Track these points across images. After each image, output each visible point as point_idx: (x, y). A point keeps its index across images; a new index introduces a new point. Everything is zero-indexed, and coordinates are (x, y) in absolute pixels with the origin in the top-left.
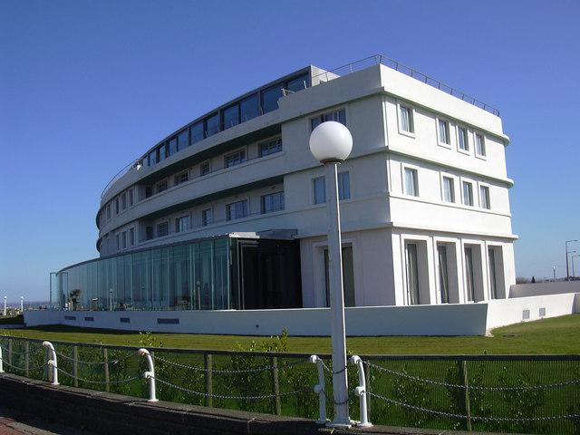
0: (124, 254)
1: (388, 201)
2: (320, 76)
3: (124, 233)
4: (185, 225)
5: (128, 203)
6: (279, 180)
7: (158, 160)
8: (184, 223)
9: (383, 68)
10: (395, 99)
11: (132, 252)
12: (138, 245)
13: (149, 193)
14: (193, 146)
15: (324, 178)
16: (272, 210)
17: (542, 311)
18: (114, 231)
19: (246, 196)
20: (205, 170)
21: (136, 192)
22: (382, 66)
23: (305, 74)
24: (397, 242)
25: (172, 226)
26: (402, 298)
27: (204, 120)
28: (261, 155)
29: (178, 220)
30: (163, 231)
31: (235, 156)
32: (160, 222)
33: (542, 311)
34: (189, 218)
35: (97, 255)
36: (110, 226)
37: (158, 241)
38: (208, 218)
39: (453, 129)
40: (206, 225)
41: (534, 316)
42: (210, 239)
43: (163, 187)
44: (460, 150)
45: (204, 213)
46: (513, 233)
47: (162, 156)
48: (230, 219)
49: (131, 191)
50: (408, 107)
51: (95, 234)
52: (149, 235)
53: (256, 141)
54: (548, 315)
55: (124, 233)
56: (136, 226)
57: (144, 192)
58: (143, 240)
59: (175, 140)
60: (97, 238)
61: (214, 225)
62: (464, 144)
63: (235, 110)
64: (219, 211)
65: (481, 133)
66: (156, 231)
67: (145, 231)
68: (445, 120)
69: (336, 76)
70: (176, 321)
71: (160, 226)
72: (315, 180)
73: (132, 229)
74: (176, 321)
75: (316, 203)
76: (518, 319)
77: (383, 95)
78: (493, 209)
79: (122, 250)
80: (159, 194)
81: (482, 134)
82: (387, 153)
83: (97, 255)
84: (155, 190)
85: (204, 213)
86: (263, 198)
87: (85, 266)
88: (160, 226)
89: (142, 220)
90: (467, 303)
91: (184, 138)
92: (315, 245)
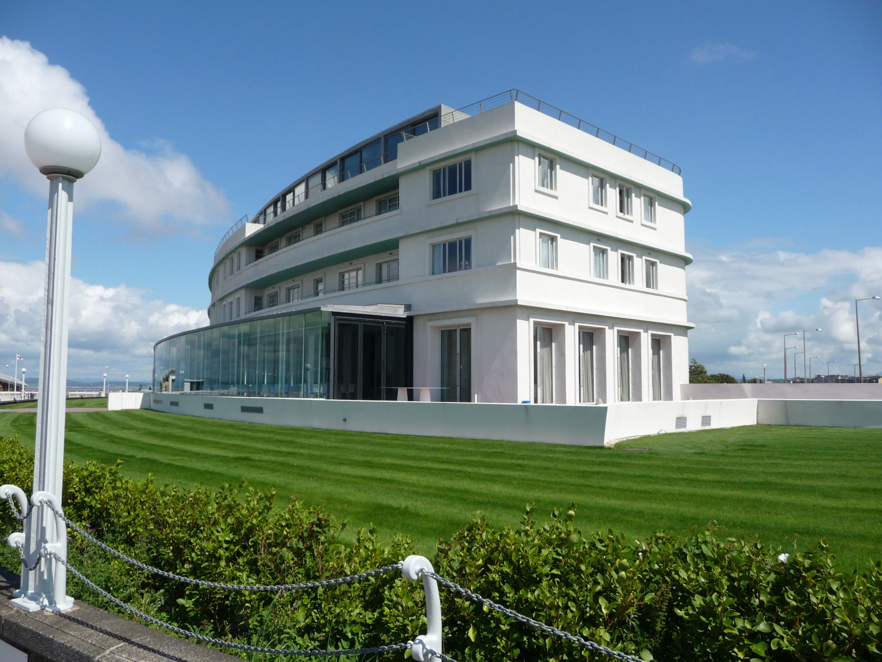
2: (450, 116)
3: (231, 303)
4: (296, 295)
5: (235, 267)
6: (391, 246)
8: (295, 293)
9: (518, 106)
13: (259, 255)
15: (468, 242)
16: (389, 280)
17: (706, 420)
20: (319, 230)
23: (433, 118)
25: (282, 295)
26: (525, 393)
29: (289, 290)
30: (273, 301)
31: (351, 214)
32: (270, 291)
33: (706, 420)
34: (360, 272)
40: (343, 290)
41: (694, 425)
46: (689, 320)
47: (279, 210)
48: (317, 294)
51: (207, 298)
52: (258, 304)
54: (715, 425)
56: (242, 295)
57: (254, 254)
58: (250, 312)
59: (358, 154)
63: (356, 159)
65: (651, 195)
66: (265, 301)
69: (469, 116)
72: (434, 246)
73: (238, 299)
75: (433, 274)
76: (670, 428)
78: (662, 288)
79: (235, 319)
81: (653, 197)
84: (266, 251)
90: (578, 404)
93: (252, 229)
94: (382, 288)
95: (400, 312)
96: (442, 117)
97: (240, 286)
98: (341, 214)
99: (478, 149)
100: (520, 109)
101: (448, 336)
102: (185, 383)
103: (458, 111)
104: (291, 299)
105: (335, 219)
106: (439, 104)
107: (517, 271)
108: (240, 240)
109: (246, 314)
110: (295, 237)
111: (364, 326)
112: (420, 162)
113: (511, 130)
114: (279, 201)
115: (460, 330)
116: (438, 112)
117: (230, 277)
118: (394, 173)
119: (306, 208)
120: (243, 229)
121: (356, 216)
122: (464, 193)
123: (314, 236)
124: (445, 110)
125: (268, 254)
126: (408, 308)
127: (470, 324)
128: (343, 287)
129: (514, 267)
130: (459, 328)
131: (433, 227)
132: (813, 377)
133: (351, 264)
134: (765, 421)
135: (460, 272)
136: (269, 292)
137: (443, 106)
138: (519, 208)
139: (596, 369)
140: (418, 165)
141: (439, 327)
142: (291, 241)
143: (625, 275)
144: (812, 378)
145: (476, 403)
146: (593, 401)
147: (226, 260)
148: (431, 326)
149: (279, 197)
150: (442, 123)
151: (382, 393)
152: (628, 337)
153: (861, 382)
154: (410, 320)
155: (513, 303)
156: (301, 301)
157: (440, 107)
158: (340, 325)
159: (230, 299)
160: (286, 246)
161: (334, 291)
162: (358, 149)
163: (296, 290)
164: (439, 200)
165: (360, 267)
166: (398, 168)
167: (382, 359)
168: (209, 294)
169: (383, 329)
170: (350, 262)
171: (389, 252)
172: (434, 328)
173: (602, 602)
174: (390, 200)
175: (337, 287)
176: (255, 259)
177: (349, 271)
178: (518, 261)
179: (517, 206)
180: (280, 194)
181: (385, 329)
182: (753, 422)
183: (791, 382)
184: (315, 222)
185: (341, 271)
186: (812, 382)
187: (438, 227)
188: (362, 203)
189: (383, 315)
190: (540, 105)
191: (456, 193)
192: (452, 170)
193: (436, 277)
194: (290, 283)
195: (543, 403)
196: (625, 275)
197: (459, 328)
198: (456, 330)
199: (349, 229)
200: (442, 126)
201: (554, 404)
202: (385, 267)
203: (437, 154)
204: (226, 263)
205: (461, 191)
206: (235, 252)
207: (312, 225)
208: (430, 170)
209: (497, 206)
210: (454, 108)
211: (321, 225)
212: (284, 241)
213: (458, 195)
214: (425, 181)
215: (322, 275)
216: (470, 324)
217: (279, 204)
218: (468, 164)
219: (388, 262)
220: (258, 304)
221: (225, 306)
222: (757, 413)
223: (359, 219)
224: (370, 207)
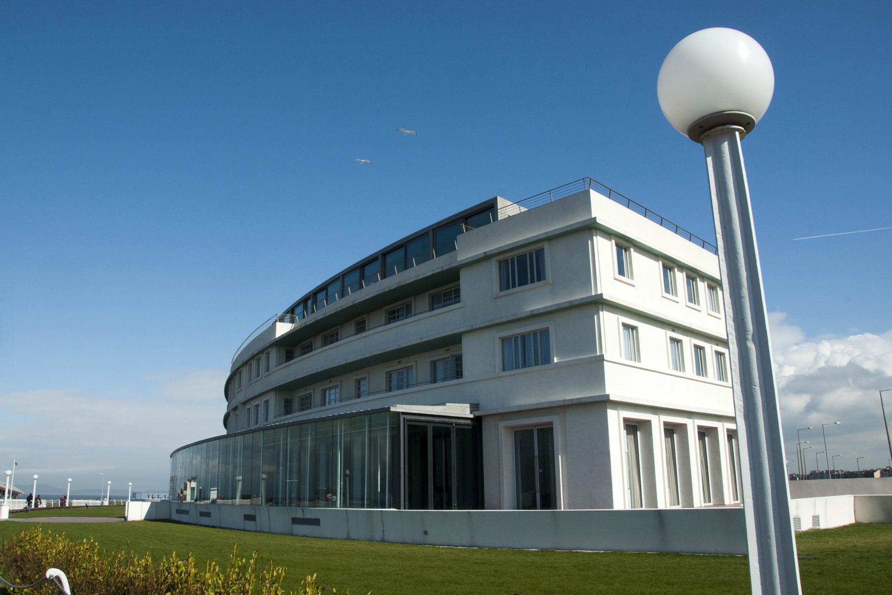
0: (253, 431)
1: (603, 363)
2: (507, 209)
3: (257, 406)
4: (333, 397)
6: (455, 340)
7: (343, 294)
8: (333, 394)
10: (609, 234)
11: (264, 429)
12: (273, 420)
13: (289, 356)
14: (345, 298)
18: (245, 403)
19: (406, 363)
20: (361, 328)
21: (274, 355)
22: (591, 190)
23: (490, 207)
24: (615, 419)
25: (317, 398)
26: (621, 500)
27: (385, 254)
28: (432, 309)
29: (324, 391)
30: (306, 404)
32: (302, 393)
33: (816, 519)
34: (338, 390)
35: (224, 432)
36: (241, 397)
37: (298, 416)
38: (362, 389)
39: (680, 277)
42: (366, 413)
43: (308, 349)
44: (690, 304)
45: (358, 382)
48: (324, 405)
49: (268, 354)
50: (624, 244)
51: (222, 407)
52: (288, 408)
53: (381, 308)
54: (823, 526)
55: (257, 406)
56: (272, 398)
57: (284, 353)
58: (280, 416)
59: (324, 292)
60: (224, 410)
61: (371, 397)
62: (693, 297)
64: (378, 377)
66: (296, 404)
67: (283, 404)
68: (669, 264)
70: (316, 522)
71: (302, 399)
72: (503, 340)
73: (267, 402)
74: (316, 522)
75: (504, 370)
77: (592, 228)
80: (324, 348)
82: (599, 303)
83: (224, 432)
85: (358, 382)
86: (434, 364)
87: (205, 444)
88: (302, 399)
89: (279, 389)
91: (335, 289)
92: (502, 424)
93: (283, 329)
94: (418, 391)
95: (461, 410)
96: (499, 211)
97: (270, 388)
98: (431, 294)
99: (551, 238)
100: (595, 196)
101: (523, 438)
102: (211, 492)
103: (515, 205)
104: (327, 401)
105: (381, 316)
106: (495, 196)
107: (605, 362)
108: (267, 343)
109: (275, 417)
110: (308, 346)
111: (433, 427)
112: (485, 252)
113: (588, 218)
114: (310, 299)
115: (537, 429)
116: (493, 204)
117: (256, 380)
118: (455, 264)
119: (350, 304)
120: (273, 328)
121: (310, 349)
122: (537, 284)
123: (355, 334)
124: (501, 202)
125: (300, 356)
126: (474, 407)
127: (551, 423)
128: (390, 387)
129: (601, 359)
130: (537, 428)
131: (504, 320)
132: (808, 473)
133: (399, 362)
134: (864, 519)
135: (517, 370)
136: (301, 394)
137: (499, 199)
138: (604, 297)
139: (710, 469)
140: (482, 256)
141: (512, 428)
142: (393, 317)
143: (701, 368)
144: (808, 474)
145: (562, 510)
146: (679, 504)
147: (252, 361)
148: (504, 427)
149: (310, 296)
150: (499, 216)
151: (453, 501)
152: (704, 433)
153: (840, 478)
154: (478, 421)
155: (605, 399)
156: (338, 404)
157: (496, 199)
158: (409, 426)
159: (255, 403)
160: (321, 347)
161: (351, 399)
162: (325, 286)
163: (333, 391)
164: (509, 291)
165: (412, 365)
166: (458, 260)
167: (453, 465)
168: (225, 403)
169: (452, 431)
170: (447, 348)
171: (329, 380)
172: (506, 428)
173: (240, 562)
174: (331, 336)
175: (384, 387)
176: (285, 360)
177: (330, 389)
178: (604, 353)
179: (601, 294)
180: (289, 308)
181: (455, 430)
182: (853, 521)
183: (798, 479)
184: (357, 319)
185: (388, 370)
186: (808, 479)
187: (266, 390)
188: (412, 298)
189: (452, 416)
190: (610, 193)
191: (527, 284)
192: (522, 259)
193: (507, 373)
194: (326, 385)
195: (634, 508)
196: (701, 368)
197: (537, 428)
198: (532, 431)
199: (402, 325)
200: (499, 219)
201: (644, 508)
202: (395, 377)
203: (522, 239)
204: (251, 364)
205: (532, 281)
206: (263, 352)
207: (427, 294)
208: (496, 260)
209: (579, 296)
210: (512, 201)
211: (364, 322)
212: (318, 341)
213: (530, 286)
214: (492, 271)
215: (311, 391)
216: (551, 423)
217: (310, 302)
218: (540, 253)
219: (444, 359)
220: (288, 408)
221: (249, 409)
222: (855, 511)
223: (337, 340)
224: (423, 302)
